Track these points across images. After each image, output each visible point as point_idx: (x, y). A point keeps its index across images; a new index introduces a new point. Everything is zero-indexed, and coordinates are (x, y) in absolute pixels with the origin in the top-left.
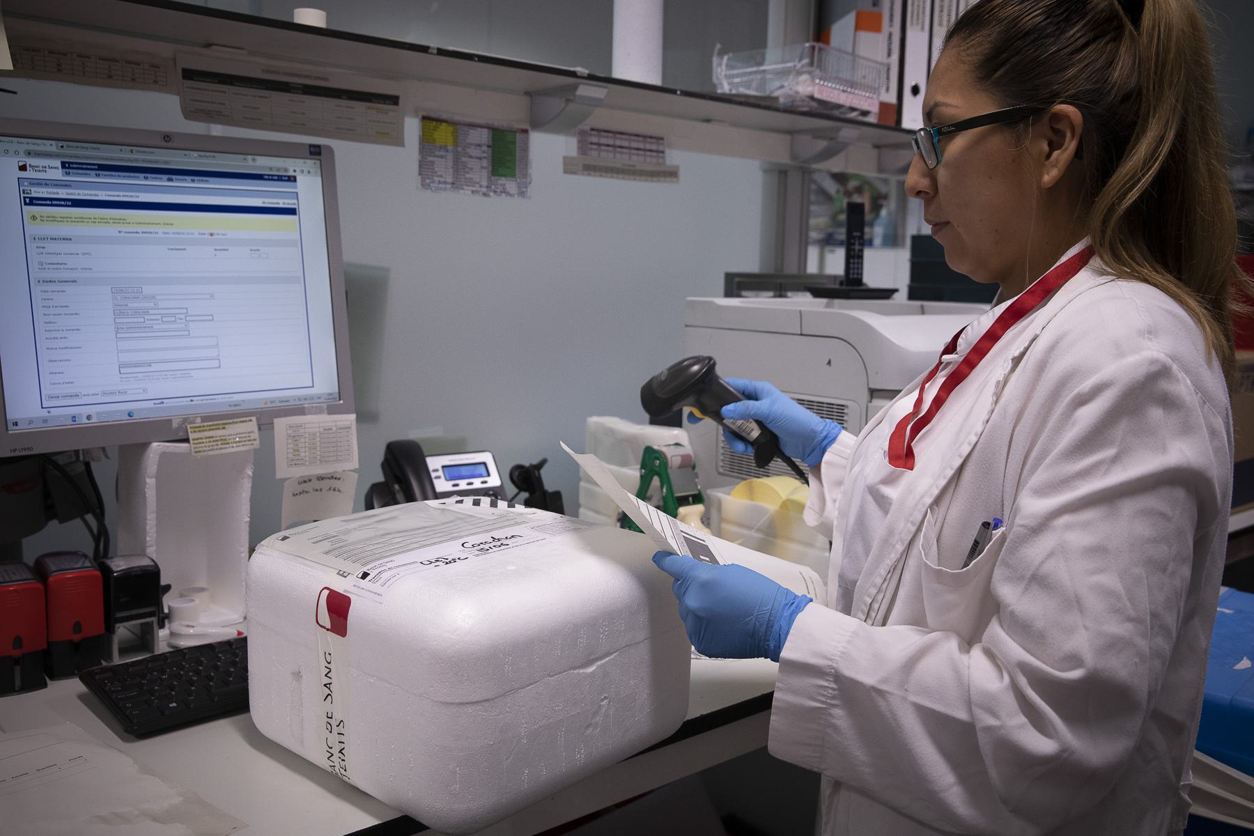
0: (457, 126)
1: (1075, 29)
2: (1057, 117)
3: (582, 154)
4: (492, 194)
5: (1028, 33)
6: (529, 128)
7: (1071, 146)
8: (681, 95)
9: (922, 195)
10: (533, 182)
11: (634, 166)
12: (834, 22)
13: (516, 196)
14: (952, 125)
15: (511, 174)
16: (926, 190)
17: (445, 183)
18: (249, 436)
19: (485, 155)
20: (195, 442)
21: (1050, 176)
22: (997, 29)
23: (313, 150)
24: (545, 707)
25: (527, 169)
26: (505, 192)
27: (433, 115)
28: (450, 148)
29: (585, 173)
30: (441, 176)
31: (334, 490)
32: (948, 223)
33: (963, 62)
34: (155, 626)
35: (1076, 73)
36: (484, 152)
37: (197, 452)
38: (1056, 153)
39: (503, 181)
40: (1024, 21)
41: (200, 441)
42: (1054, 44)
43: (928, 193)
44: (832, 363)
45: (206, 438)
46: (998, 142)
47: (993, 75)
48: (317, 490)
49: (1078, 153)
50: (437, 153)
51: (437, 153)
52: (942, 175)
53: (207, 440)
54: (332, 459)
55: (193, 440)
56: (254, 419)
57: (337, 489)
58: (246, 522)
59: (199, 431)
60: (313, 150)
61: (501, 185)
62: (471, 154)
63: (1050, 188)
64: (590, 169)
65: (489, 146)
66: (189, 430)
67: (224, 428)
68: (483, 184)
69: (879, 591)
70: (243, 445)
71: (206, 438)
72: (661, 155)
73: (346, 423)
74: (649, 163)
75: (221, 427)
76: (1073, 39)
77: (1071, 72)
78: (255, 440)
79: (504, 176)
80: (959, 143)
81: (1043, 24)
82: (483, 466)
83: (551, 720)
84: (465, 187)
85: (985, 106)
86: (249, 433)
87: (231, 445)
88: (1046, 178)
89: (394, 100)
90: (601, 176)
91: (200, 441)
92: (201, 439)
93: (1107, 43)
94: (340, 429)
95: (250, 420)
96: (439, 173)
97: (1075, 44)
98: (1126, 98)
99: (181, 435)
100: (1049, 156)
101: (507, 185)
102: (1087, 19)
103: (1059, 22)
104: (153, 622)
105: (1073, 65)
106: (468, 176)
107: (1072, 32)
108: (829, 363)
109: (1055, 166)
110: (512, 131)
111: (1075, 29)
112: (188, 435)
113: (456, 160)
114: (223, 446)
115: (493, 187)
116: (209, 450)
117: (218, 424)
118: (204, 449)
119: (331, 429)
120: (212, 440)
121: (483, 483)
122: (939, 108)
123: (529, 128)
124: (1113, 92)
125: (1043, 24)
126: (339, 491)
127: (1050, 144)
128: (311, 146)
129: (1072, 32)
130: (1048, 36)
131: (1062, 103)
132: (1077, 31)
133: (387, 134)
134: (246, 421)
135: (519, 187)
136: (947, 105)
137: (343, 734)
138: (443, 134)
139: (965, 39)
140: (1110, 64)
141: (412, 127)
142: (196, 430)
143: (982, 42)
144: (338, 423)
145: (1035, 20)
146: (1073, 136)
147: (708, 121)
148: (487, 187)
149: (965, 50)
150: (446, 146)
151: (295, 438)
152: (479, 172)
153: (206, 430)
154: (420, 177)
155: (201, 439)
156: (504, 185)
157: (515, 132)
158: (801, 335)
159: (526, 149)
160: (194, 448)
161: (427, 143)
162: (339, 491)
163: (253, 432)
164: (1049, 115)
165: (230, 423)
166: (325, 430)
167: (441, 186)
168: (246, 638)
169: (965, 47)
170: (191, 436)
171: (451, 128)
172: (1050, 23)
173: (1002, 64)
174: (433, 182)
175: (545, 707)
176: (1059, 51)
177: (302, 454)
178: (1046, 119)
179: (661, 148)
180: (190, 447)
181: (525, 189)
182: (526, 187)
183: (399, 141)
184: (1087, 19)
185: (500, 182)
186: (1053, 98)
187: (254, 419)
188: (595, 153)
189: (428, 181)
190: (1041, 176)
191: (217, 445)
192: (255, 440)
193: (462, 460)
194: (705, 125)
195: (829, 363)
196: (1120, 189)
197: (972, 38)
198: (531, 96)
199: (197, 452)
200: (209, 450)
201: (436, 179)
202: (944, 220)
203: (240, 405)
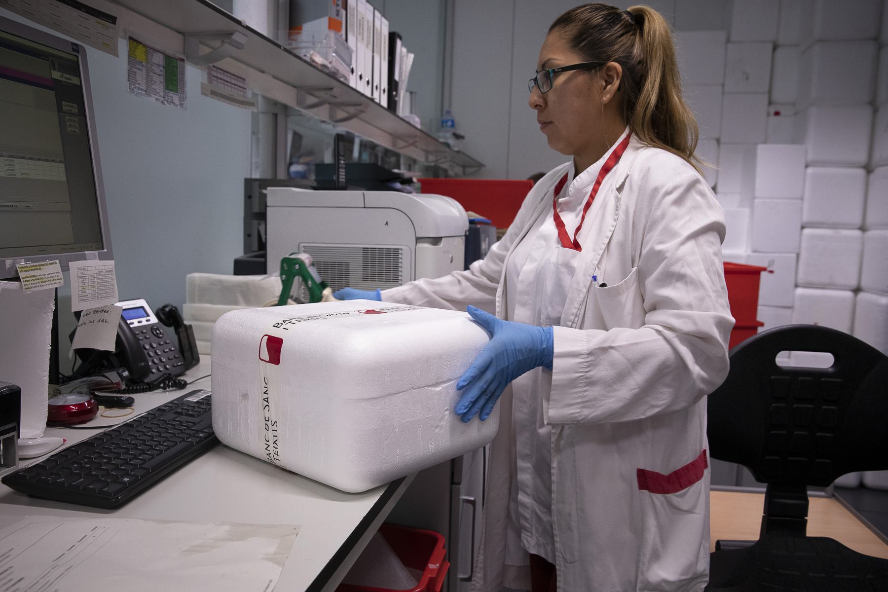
0: (150, 50)
1: (618, 27)
2: (609, 69)
3: (210, 83)
4: (166, 102)
5: (595, 26)
6: (185, 58)
7: (617, 83)
8: (283, 50)
9: (538, 107)
10: (187, 98)
11: (233, 96)
12: (305, 22)
13: (179, 106)
14: (560, 68)
15: (176, 91)
16: (541, 104)
17: (142, 89)
18: (58, 276)
19: (162, 73)
20: (24, 280)
21: (606, 98)
22: (580, 23)
23: (74, 47)
24: (410, 409)
25: (184, 87)
26: (172, 103)
27: (135, 38)
28: (144, 64)
29: (212, 96)
30: (140, 84)
31: (103, 321)
32: (551, 122)
33: (563, 38)
34: (16, 437)
35: (619, 48)
36: (161, 71)
37: (26, 288)
38: (609, 87)
39: (171, 94)
40: (594, 20)
41: (27, 279)
42: (608, 32)
43: (541, 106)
44: (389, 223)
45: (31, 277)
46: (581, 79)
47: (579, 45)
48: (91, 322)
49: (619, 89)
50: (138, 66)
51: (138, 66)
52: (552, 97)
53: (32, 278)
54: (104, 295)
55: (23, 278)
56: (57, 261)
57: (104, 320)
58: (49, 350)
59: (25, 271)
60: (74, 47)
61: (170, 97)
62: (155, 71)
63: (606, 104)
64: (214, 93)
65: (163, 67)
66: (18, 270)
67: (40, 269)
68: (161, 94)
69: (579, 309)
70: (55, 283)
71: (31, 277)
72: (245, 90)
73: (109, 267)
74: (235, 93)
75: (38, 268)
76: (616, 32)
77: (616, 47)
78: (61, 279)
79: (172, 90)
80: (562, 78)
81: (603, 22)
82: (141, 309)
83: (413, 419)
84: (152, 95)
85: (574, 59)
86: (57, 273)
87: (47, 283)
88: (604, 99)
89: (113, 20)
90: (213, 98)
91: (27, 279)
92: (27, 277)
93: (631, 36)
94: (108, 271)
95: (56, 263)
96: (139, 82)
97: (617, 34)
98: (640, 62)
99: (12, 275)
100: (605, 88)
101: (174, 98)
102: (622, 23)
103: (609, 23)
104: (14, 436)
105: (617, 43)
106: (154, 87)
107: (616, 28)
108: (387, 223)
109: (608, 93)
110: (174, 58)
111: (618, 27)
112: (18, 274)
113: (147, 74)
114: (43, 284)
115: (166, 98)
116: (35, 287)
117: (36, 266)
118: (32, 286)
119: (102, 272)
120: (34, 278)
121: (139, 322)
122: (550, 61)
123: (185, 58)
124: (634, 59)
125: (603, 22)
126: (106, 322)
127: (606, 81)
128: (73, 44)
129: (616, 28)
130: (605, 29)
131: (612, 61)
132: (619, 28)
133: (109, 45)
134: (53, 264)
135: (180, 100)
136: (555, 59)
137: (13, 549)
138: (140, 52)
139: (563, 28)
140: (633, 45)
141: (123, 46)
142: (23, 270)
143: (572, 30)
144: (97, 268)
145: (599, 20)
146: (617, 79)
147: (263, 72)
148: (163, 97)
149: (564, 33)
150: (142, 62)
151: (82, 278)
152: (159, 85)
153: (29, 270)
154: (128, 82)
155: (27, 277)
156: (172, 97)
157: (178, 60)
158: (365, 207)
159: (183, 74)
160: (25, 285)
161: (131, 55)
162: (106, 322)
163: (59, 273)
164: (606, 67)
165: (43, 265)
166: (99, 272)
167: (139, 91)
168: (208, 401)
169: (564, 31)
170: (21, 275)
171: (144, 49)
172: (605, 23)
173: (584, 40)
174: (135, 88)
175: (410, 409)
176: (610, 36)
177: (87, 292)
178: (605, 69)
179: (245, 86)
180: (21, 286)
181: (183, 102)
182: (184, 101)
183: (114, 52)
184: (622, 23)
185: (170, 95)
186: (608, 59)
187: (57, 261)
188: (215, 83)
189: (133, 86)
190: (602, 97)
191: (39, 283)
192: (61, 279)
193: (129, 305)
194: (260, 73)
195: (387, 223)
196: (644, 106)
197: (567, 27)
198: (184, 36)
199: (26, 288)
200: (35, 287)
201: (137, 85)
202: (549, 121)
203: (40, 251)
